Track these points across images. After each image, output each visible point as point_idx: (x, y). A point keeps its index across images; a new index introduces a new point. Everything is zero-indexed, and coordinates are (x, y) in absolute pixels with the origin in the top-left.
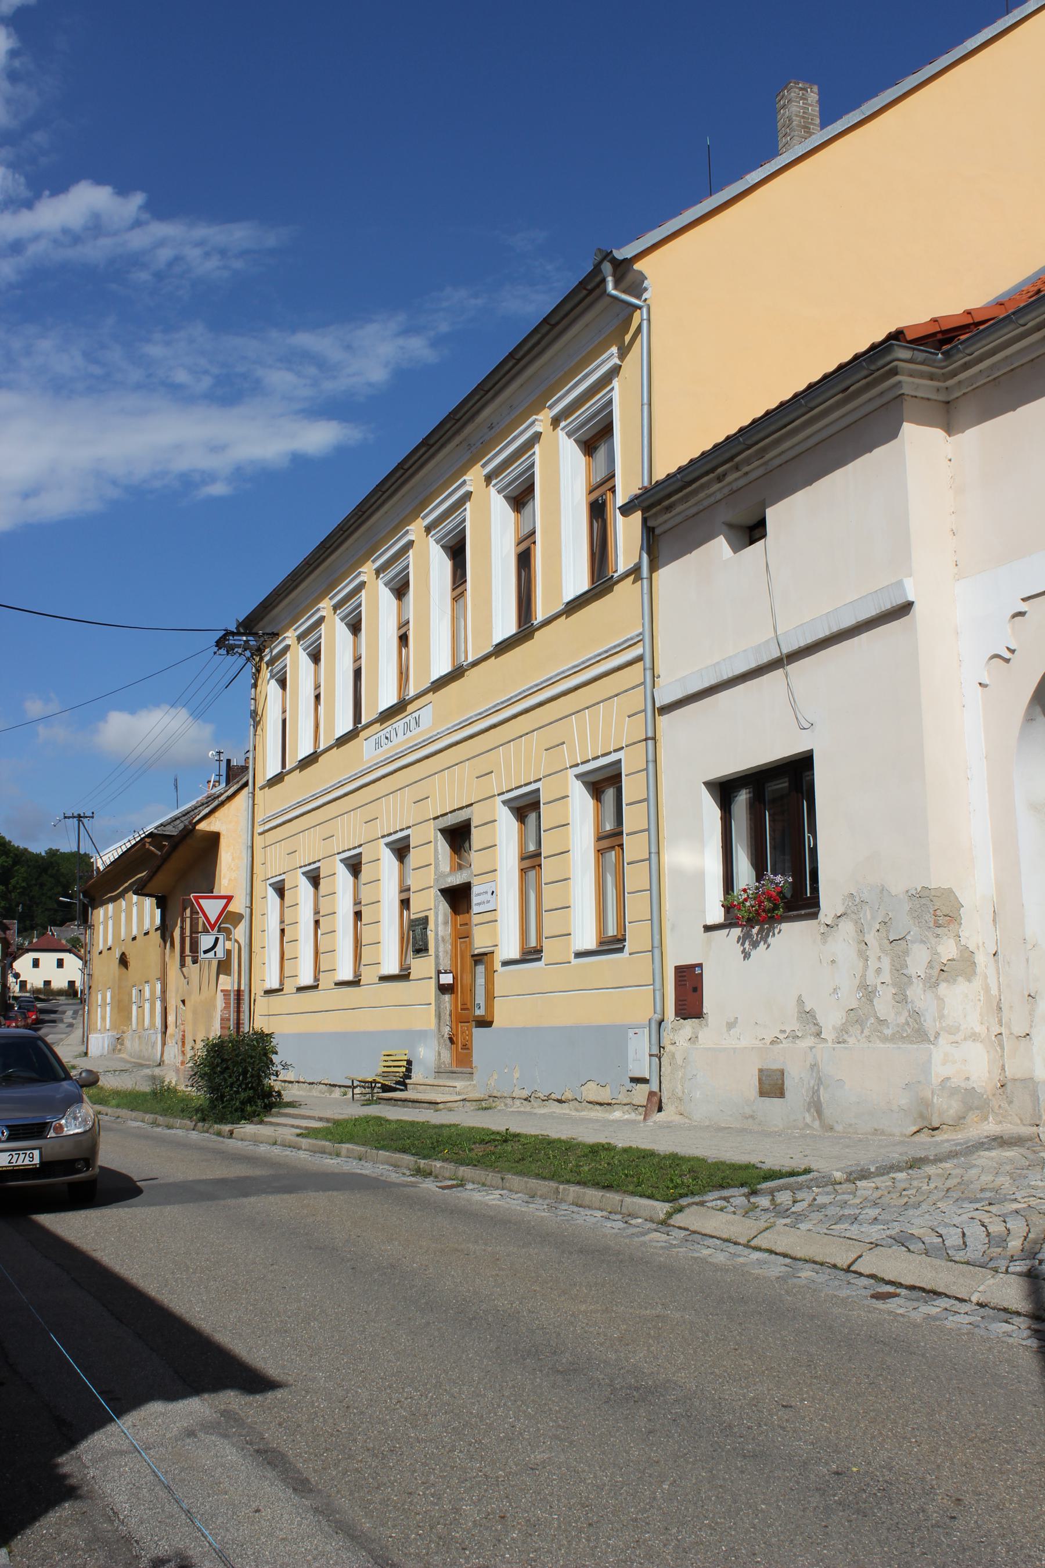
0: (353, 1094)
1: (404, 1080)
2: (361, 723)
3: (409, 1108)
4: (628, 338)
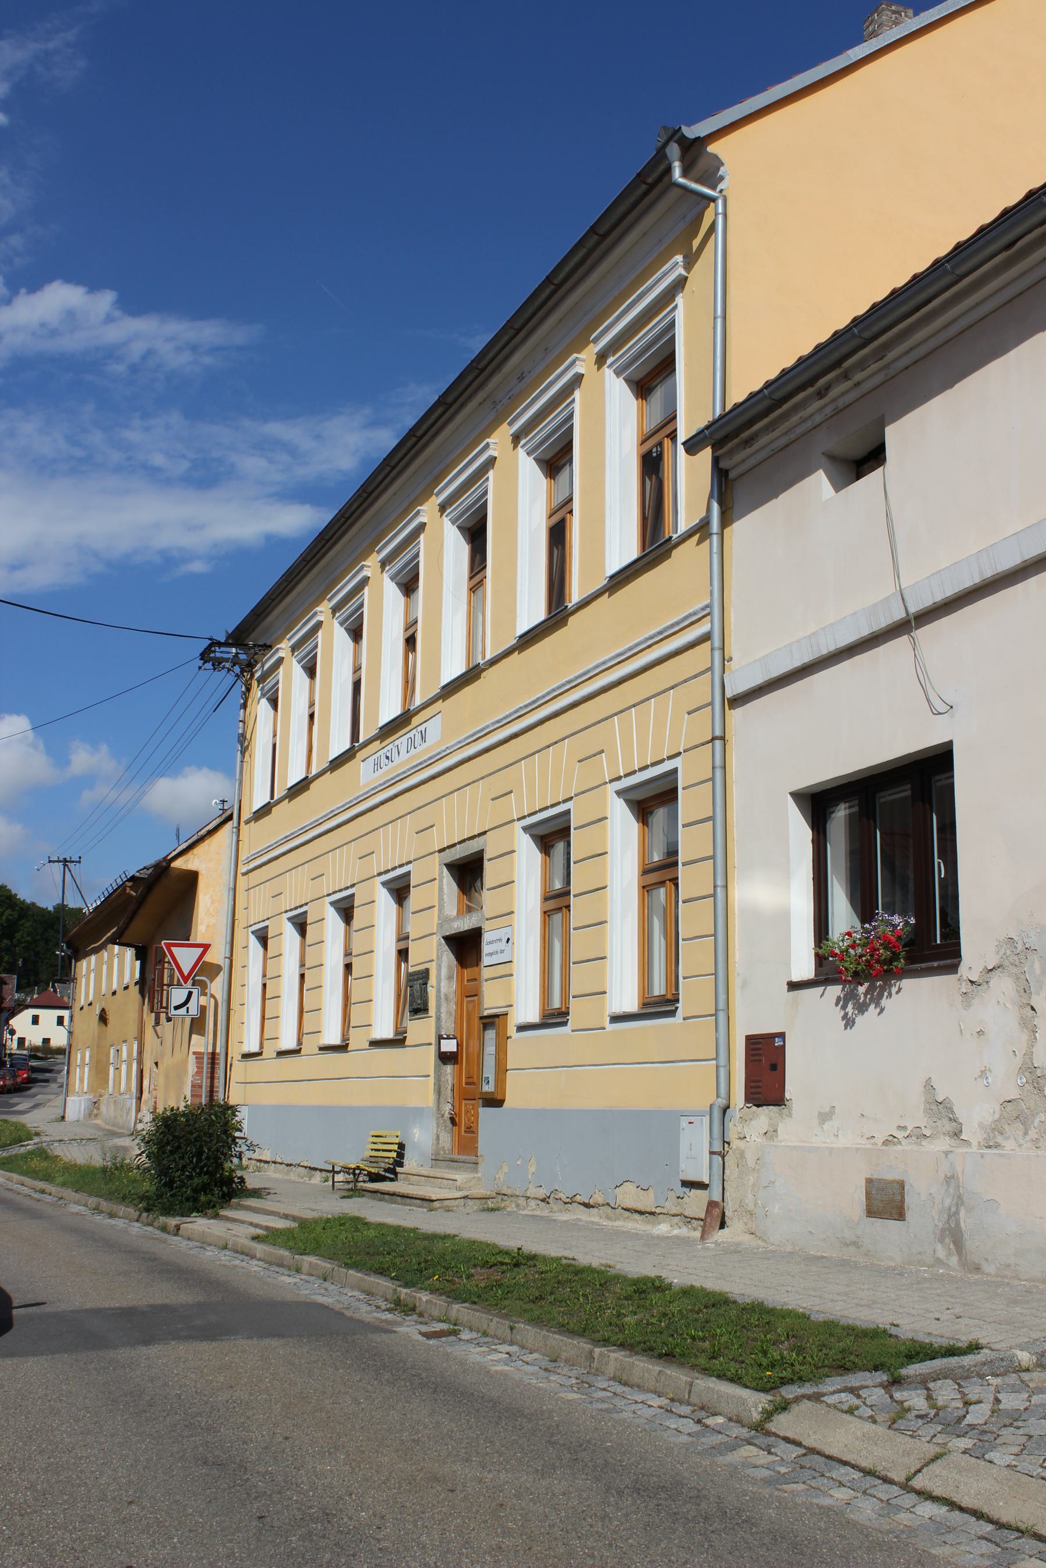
0: (333, 1182)
1: (394, 1167)
2: (358, 742)
3: (398, 1204)
4: (696, 243)
